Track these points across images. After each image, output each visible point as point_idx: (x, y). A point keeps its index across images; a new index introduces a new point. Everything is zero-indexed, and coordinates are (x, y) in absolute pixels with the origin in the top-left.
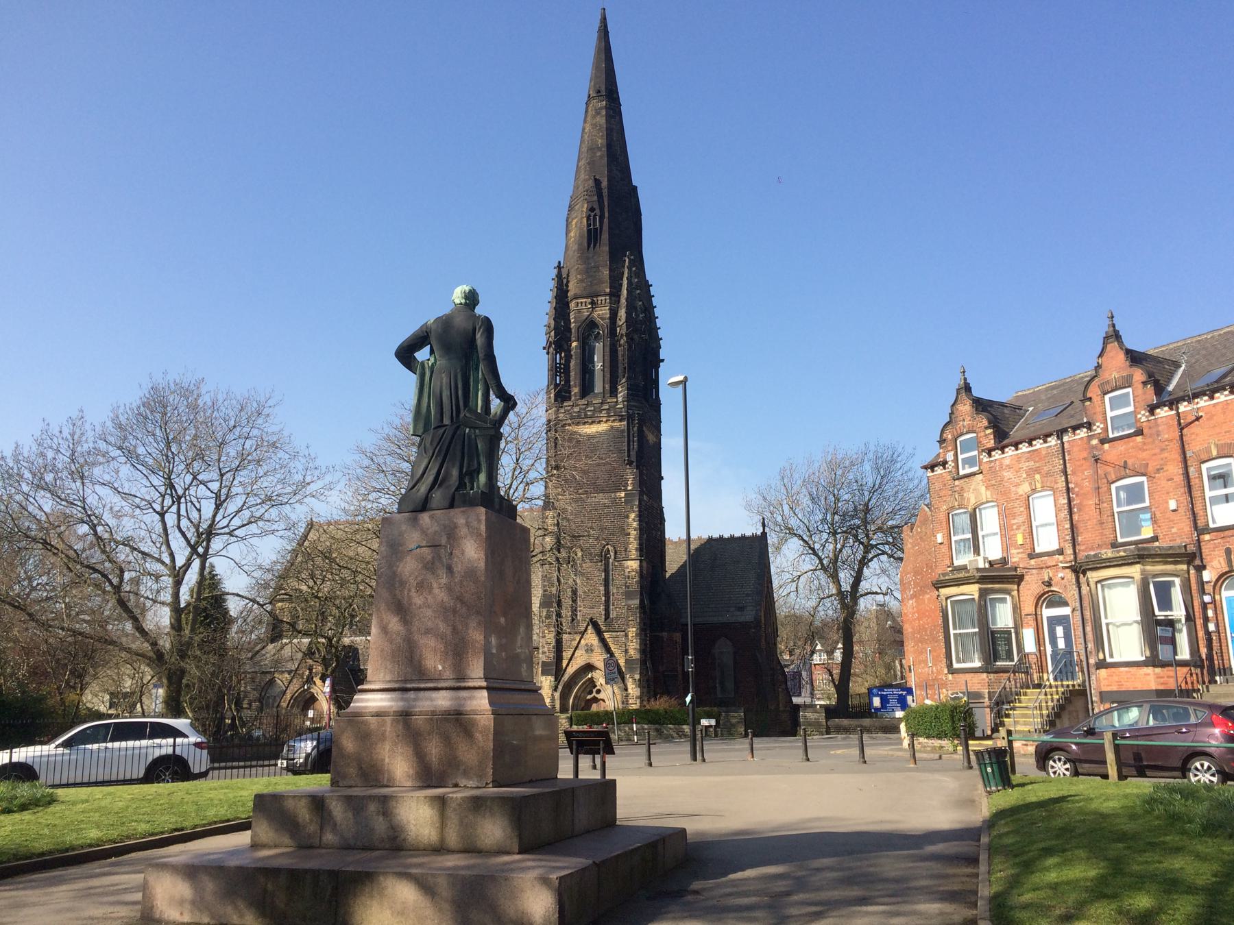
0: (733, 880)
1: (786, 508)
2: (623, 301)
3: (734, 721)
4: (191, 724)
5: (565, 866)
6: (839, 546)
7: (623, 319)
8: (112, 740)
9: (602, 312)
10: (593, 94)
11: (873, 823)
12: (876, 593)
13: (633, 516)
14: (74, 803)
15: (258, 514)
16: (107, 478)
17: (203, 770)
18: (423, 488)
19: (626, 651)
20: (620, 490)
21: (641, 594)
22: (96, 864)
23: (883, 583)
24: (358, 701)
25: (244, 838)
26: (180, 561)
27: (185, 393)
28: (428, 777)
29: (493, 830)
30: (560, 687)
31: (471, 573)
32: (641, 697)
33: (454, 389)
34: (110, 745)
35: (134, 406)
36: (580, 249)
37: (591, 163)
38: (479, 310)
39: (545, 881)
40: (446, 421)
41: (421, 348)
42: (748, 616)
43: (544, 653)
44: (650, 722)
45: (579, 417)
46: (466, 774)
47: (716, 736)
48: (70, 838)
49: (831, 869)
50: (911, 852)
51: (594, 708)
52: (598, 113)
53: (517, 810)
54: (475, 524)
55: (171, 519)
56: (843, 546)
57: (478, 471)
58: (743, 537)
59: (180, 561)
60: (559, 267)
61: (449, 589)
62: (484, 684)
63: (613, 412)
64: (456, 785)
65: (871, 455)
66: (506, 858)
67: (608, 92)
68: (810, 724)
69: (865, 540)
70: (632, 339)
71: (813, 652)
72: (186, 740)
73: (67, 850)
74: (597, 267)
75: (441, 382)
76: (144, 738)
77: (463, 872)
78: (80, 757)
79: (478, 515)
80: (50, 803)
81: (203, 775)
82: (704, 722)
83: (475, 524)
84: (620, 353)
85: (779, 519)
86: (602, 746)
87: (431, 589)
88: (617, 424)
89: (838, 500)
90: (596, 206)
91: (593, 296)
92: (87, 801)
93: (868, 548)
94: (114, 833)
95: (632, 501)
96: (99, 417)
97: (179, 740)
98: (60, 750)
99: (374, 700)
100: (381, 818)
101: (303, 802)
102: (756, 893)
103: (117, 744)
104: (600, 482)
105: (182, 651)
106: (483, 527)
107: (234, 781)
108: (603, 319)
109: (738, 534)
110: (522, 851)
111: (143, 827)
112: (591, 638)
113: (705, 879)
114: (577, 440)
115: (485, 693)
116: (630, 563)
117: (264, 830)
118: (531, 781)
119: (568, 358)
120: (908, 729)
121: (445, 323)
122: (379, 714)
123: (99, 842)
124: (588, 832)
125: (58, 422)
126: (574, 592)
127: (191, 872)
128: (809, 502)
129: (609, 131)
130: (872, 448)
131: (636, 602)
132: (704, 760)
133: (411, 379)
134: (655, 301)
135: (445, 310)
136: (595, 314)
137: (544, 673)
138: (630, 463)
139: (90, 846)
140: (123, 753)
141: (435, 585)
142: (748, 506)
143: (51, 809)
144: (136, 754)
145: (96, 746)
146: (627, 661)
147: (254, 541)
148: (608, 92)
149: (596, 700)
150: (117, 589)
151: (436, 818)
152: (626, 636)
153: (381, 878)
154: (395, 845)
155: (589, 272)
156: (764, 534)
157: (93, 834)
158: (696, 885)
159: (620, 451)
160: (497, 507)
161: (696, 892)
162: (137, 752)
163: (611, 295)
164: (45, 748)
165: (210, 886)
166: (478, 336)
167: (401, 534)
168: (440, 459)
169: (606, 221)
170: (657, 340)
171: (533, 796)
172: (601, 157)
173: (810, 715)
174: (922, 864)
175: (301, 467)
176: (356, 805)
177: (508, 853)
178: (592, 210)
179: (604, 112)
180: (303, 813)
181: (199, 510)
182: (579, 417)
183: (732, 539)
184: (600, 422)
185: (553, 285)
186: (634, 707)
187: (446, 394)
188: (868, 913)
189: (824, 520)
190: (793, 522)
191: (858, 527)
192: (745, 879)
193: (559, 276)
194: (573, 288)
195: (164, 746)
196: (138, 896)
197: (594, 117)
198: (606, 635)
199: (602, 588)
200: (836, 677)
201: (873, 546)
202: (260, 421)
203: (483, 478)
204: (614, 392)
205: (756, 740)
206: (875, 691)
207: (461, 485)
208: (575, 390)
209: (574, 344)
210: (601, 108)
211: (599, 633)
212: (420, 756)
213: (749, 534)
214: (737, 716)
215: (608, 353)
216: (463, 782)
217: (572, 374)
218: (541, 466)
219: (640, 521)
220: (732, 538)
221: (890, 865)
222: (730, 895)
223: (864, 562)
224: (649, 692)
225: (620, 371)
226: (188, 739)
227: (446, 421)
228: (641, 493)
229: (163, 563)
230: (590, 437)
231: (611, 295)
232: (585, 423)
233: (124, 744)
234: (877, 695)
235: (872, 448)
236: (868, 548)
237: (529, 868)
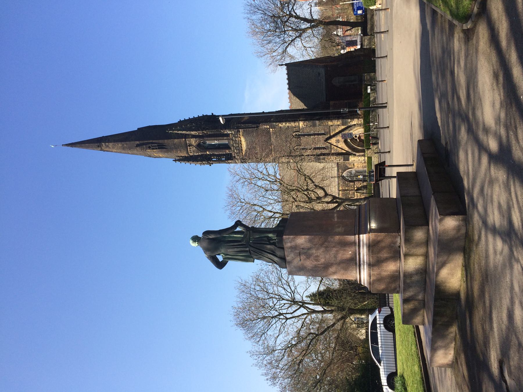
0: (442, 125)
1: (274, 54)
2: (188, 133)
3: (368, 77)
4: (371, 314)
5: (434, 209)
6: (290, 29)
7: (196, 132)
8: (378, 345)
9: (193, 141)
10: (100, 149)
11: (416, 46)
12: (311, 10)
13: (280, 125)
14: (404, 369)
15: (285, 282)
16: (273, 339)
17: (389, 310)
18: (276, 259)
19: (339, 125)
20: (269, 131)
21: (314, 120)
22: (429, 370)
23: (306, 7)
24: (364, 283)
25: (421, 328)
26: (305, 311)
27: (237, 314)
28: (396, 255)
29: (419, 235)
30: (354, 153)
31: (310, 241)
32: (358, 118)
33: (234, 247)
34: (380, 346)
35: (244, 332)
36: (167, 152)
37: (130, 148)
38: (200, 235)
39: (441, 220)
40: (248, 249)
41: (217, 259)
42: (322, 71)
43: (340, 160)
44: (369, 115)
45: (239, 150)
46: (395, 243)
47: (375, 85)
48: (418, 377)
49: (437, 78)
50: (430, 35)
51: (363, 138)
52: (108, 146)
53: (410, 226)
54: (290, 240)
55: (288, 316)
56: (290, 27)
57: (268, 237)
58: (288, 74)
59: (305, 311)
60: (175, 160)
61: (318, 249)
62: (357, 236)
63: (236, 135)
64: (399, 247)
65: (249, 16)
66: (431, 231)
67: (98, 142)
68: (370, 43)
69: (287, 17)
70: (204, 128)
71: (337, 35)
72: (378, 317)
73: (423, 380)
74: (174, 144)
75: (231, 251)
76: (377, 333)
77: (437, 252)
78: (384, 357)
79: (286, 239)
80: (404, 378)
81: (392, 309)
82: (369, 91)
83: (290, 240)
84: (211, 133)
85: (279, 57)
86: (381, 167)
87: (317, 256)
88: (241, 133)
89: (270, 30)
90: (148, 146)
91: (186, 146)
92: (403, 363)
93: (291, 16)
94: (416, 360)
95: (274, 125)
96: (249, 345)
97: (378, 322)
98: (382, 364)
99: (364, 274)
100: (413, 278)
101: (406, 307)
102: (448, 117)
103: (380, 343)
104: (266, 139)
105: (341, 309)
106: (292, 237)
107: (394, 300)
108: (196, 141)
109: (286, 77)
110: (428, 225)
111: (414, 347)
112: (333, 141)
113: (440, 137)
114: (249, 148)
115: (361, 236)
116: (301, 125)
117: (417, 320)
118: (398, 212)
119: (214, 155)
120: (372, 5)
121: (206, 250)
122: (370, 276)
123: (420, 366)
124: (419, 187)
125: (252, 361)
126: (315, 148)
127: (434, 350)
128: (271, 44)
129: (115, 141)
130: (246, 15)
131: (317, 122)
132: (386, 103)
133: (230, 263)
134: (187, 118)
135: (201, 250)
136: (194, 144)
137: (348, 160)
138: (258, 127)
139: (421, 371)
140: (383, 341)
141: (316, 254)
142: (274, 71)
143: (406, 378)
144: (384, 338)
145: (380, 351)
146: (343, 125)
147: (296, 284)
148: (98, 142)
149: (359, 137)
150: (317, 335)
151: (413, 258)
152: (332, 126)
153: (438, 283)
154: (424, 272)
155: (176, 148)
156: (286, 65)
157: (416, 368)
158: (443, 142)
159: (252, 132)
160: (282, 229)
161: (446, 144)
162: (383, 338)
163: (185, 138)
164: (381, 370)
165: (439, 343)
166: (211, 237)
167: (295, 267)
168: (263, 252)
169: (154, 141)
170: (204, 116)
171: (404, 215)
172: (126, 144)
173: (366, 43)
174: (436, 36)
175: (266, 267)
176: (407, 286)
177: (428, 230)
178: (149, 148)
179: (107, 144)
180: (410, 306)
181: (285, 304)
182: (239, 150)
183: (288, 79)
184: (241, 141)
185: (183, 163)
186: (362, 121)
187: (236, 250)
188: (458, 75)
189: (279, 37)
190: (280, 51)
191: (281, 21)
192: (441, 119)
193: (179, 160)
194: (184, 154)
195: (381, 329)
196: (443, 369)
197: (109, 148)
198: (332, 134)
199: (312, 137)
200: (349, 28)
201: (290, 13)
202: (247, 284)
203: (270, 235)
204: (228, 135)
205: (376, 56)
206: (355, 13)
207: (274, 244)
208: (227, 152)
209: (208, 153)
210: (106, 145)
211: (331, 137)
212: (386, 260)
213: (286, 72)
214: (366, 76)
215: (211, 139)
216: (398, 244)
217: (220, 153)
218: (261, 166)
219: (282, 122)
220: (288, 79)
221: (436, 51)
222: (448, 132)
223: (297, 17)
224: (356, 115)
225: (218, 133)
226: (378, 316)
227: (248, 249)
228: (271, 122)
229: (306, 318)
230: (247, 145)
231: (185, 138)
232: (241, 147)
233: (379, 338)
234: (357, 12)
235: (246, 15)
236: (291, 16)
237: (436, 225)
